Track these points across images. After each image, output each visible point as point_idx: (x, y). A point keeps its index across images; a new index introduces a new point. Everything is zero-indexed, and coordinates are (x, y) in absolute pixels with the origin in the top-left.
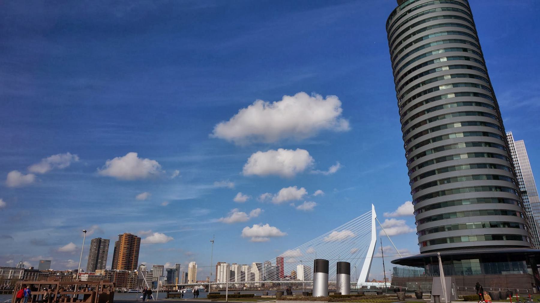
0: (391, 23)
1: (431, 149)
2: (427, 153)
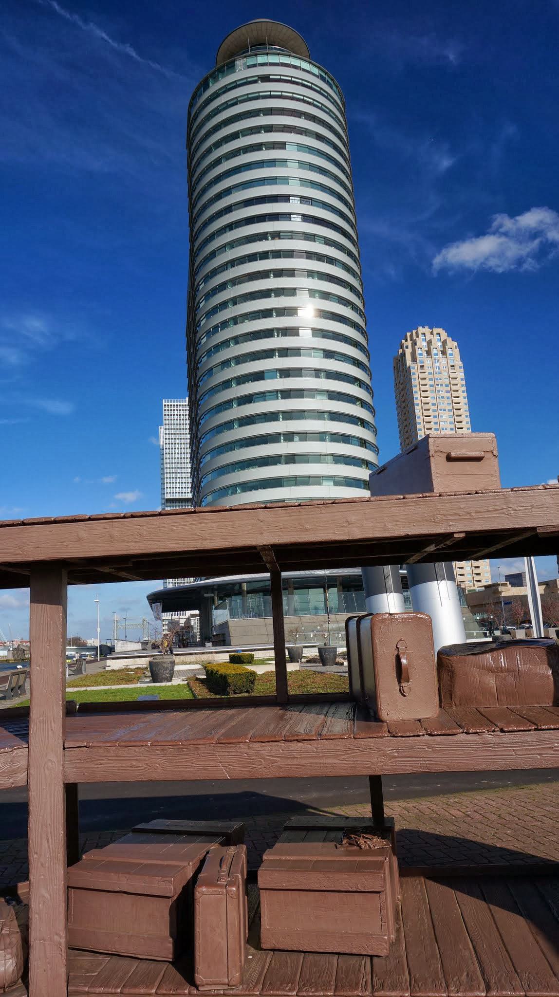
0: (214, 88)
1: (277, 391)
2: (266, 375)
